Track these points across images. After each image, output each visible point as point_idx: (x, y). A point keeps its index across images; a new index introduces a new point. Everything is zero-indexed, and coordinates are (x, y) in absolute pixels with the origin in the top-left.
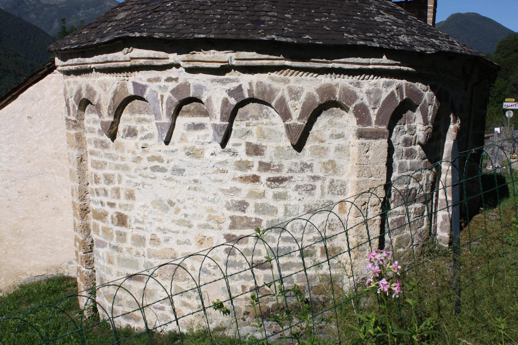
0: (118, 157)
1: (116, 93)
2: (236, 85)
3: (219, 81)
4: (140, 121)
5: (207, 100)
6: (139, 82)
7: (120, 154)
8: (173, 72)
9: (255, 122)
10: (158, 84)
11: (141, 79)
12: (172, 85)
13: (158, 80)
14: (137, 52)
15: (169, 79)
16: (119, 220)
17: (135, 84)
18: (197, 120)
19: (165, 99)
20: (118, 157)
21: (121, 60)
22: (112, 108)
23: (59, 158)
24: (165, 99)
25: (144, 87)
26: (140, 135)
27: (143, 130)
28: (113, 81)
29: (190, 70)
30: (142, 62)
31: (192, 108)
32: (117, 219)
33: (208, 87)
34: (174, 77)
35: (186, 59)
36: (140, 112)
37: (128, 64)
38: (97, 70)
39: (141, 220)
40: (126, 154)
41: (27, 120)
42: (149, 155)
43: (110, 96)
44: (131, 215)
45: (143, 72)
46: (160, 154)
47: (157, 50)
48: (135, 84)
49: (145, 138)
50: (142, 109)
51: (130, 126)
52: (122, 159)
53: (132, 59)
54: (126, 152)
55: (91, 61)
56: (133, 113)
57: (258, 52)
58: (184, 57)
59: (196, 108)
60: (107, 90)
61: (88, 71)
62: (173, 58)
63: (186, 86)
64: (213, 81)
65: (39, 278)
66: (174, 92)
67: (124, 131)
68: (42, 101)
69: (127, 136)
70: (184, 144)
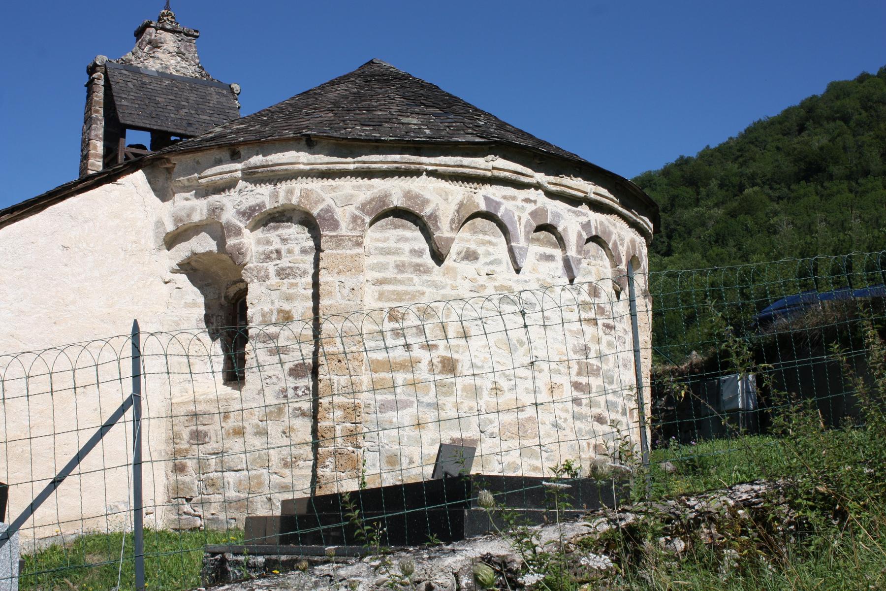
0: (447, 285)
1: (461, 205)
2: (586, 219)
3: (574, 212)
4: (484, 243)
5: (564, 230)
6: (492, 197)
7: (449, 282)
8: (532, 193)
9: (594, 262)
10: (514, 202)
11: (494, 194)
12: (531, 207)
13: (514, 198)
14: (501, 162)
15: (527, 200)
16: (444, 367)
17: (486, 199)
18: (549, 251)
19: (523, 221)
20: (447, 285)
21: (482, 167)
22: (456, 221)
23: (114, 322)
24: (523, 221)
25: (498, 204)
26: (482, 260)
27: (488, 254)
28: (458, 191)
29: (550, 195)
30: (502, 174)
31: (542, 237)
32: (440, 365)
33: (564, 216)
34: (532, 198)
35: (554, 181)
36: (485, 233)
37: (489, 174)
38: (431, 174)
39: (480, 364)
40: (459, 281)
41: (59, 252)
42: (497, 284)
43: (454, 207)
44: (464, 360)
45: (498, 187)
46: (509, 283)
47: (524, 166)
48: (486, 199)
49: (491, 263)
50: (486, 229)
51: (468, 249)
52: (454, 288)
53: (494, 168)
54: (459, 278)
55: (428, 162)
56: (475, 233)
57: (610, 191)
58: (552, 179)
59: (545, 237)
60: (450, 200)
61: (418, 173)
62: (540, 177)
63: (542, 212)
64: (569, 210)
65: (49, 542)
66: (533, 214)
67: (459, 254)
68: (91, 224)
69: (463, 259)
70: (536, 275)
